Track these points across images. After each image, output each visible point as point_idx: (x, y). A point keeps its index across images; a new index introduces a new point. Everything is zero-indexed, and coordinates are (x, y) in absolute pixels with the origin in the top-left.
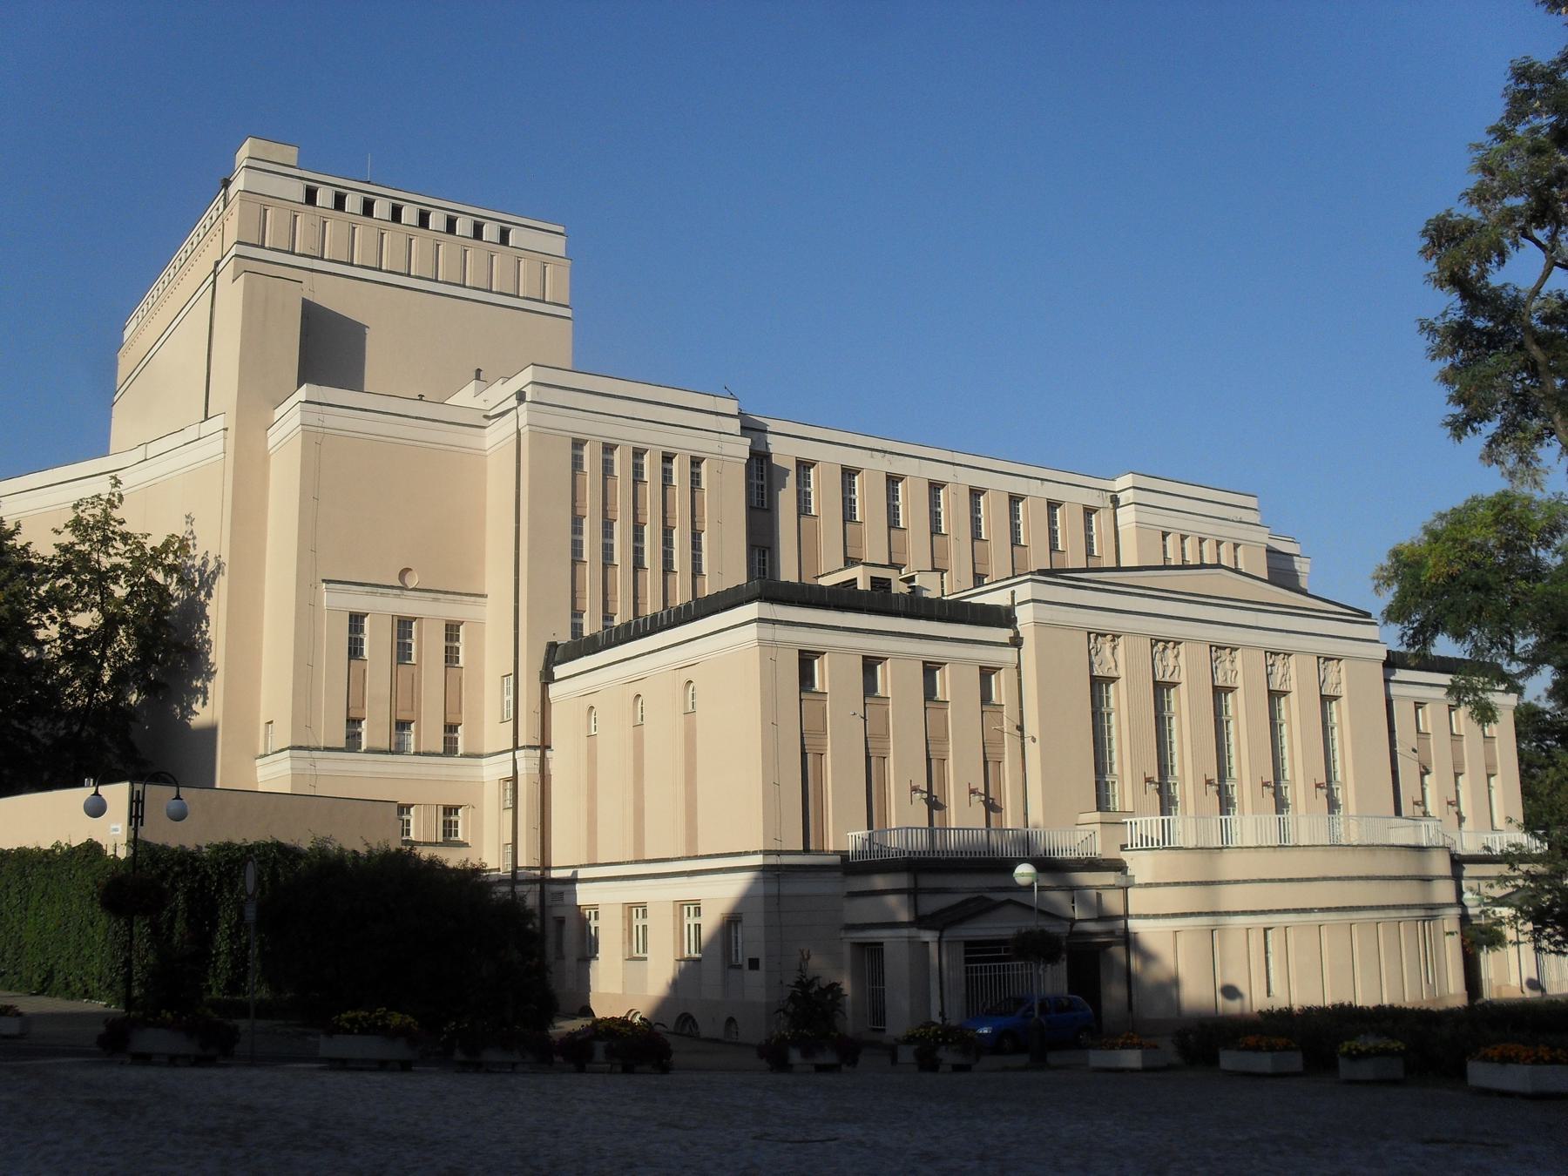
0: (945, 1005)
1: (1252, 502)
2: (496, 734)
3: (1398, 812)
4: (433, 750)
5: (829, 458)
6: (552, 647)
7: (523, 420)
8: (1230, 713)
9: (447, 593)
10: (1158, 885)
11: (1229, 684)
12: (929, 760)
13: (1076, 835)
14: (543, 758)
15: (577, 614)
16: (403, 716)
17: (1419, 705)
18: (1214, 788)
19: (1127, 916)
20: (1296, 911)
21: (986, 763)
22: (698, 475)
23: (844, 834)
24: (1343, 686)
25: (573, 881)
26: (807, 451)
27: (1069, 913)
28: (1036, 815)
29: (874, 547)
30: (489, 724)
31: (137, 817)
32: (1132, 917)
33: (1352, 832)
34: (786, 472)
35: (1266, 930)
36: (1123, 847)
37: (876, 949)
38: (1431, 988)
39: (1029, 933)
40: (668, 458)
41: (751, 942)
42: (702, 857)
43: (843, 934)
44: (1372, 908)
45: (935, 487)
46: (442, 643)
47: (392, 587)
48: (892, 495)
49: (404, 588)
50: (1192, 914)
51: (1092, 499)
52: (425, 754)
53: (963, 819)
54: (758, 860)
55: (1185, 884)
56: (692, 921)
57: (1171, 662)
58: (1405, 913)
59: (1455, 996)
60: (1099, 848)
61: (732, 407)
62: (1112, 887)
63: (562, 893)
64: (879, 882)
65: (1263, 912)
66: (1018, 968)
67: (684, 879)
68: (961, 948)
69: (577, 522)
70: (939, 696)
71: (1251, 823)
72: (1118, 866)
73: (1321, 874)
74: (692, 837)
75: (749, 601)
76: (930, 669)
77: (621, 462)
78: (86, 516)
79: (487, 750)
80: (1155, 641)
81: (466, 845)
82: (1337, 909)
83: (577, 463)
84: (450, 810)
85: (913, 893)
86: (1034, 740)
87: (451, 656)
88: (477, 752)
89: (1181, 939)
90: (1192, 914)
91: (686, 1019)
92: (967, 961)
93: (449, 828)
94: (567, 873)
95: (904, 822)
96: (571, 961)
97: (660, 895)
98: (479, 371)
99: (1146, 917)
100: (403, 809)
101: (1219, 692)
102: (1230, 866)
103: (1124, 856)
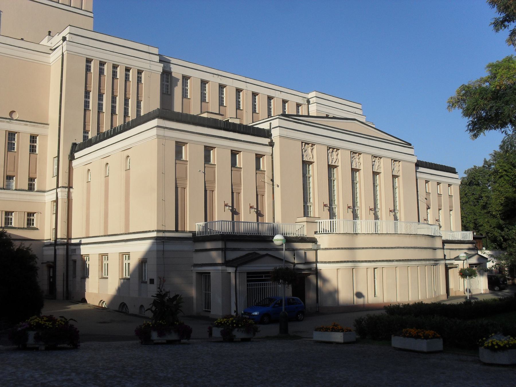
0: (237, 306)
1: (360, 106)
2: (50, 182)
3: (419, 221)
4: (23, 188)
5: (196, 75)
6: (74, 145)
7: (64, 49)
8: (358, 180)
10: (331, 249)
11: (357, 168)
12: (232, 193)
13: (298, 227)
14: (69, 193)
15: (86, 132)
16: (10, 174)
17: (427, 182)
18: (351, 210)
19: (317, 262)
20: (387, 261)
21: (257, 195)
22: (141, 78)
23: (194, 224)
24: (401, 172)
25: (80, 244)
26: (187, 72)
27: (292, 260)
28: (278, 219)
29: (213, 105)
30: (47, 179)
32: (319, 262)
33: (402, 228)
34: (178, 80)
35: (374, 269)
36: (316, 233)
37: (206, 276)
38: (435, 292)
39: (280, 269)
40: (128, 70)
41: (151, 272)
43: (192, 268)
44: (415, 260)
45: (238, 91)
46: (28, 143)
47: (6, 118)
48: (221, 93)
49: (12, 119)
50: (345, 262)
51: (300, 101)
52: (19, 190)
53: (247, 218)
54: (154, 234)
55: (342, 249)
56: (126, 262)
57: (335, 157)
58: (428, 262)
59: (443, 295)
60: (306, 233)
61: (156, 51)
62: (311, 249)
63: (75, 249)
64: (208, 245)
65: (373, 261)
66: (270, 285)
67: (123, 243)
68: (246, 275)
69: (87, 94)
70: (238, 165)
71: (364, 224)
72: (313, 241)
73: (397, 246)
74: (127, 225)
75: (153, 118)
76: (234, 153)
77: (107, 70)
79: (47, 189)
80: (329, 148)
81: (37, 229)
82: (403, 260)
84: (30, 214)
85: (224, 250)
86: (278, 186)
87: (33, 149)
88: (43, 190)
89: (340, 272)
90: (345, 262)
91: (123, 305)
92: (248, 281)
93: (30, 222)
94: (77, 241)
95: (221, 220)
96: (78, 278)
97: (114, 250)
98: (50, 32)
99: (325, 262)
101: (354, 171)
102: (360, 242)
103: (316, 236)
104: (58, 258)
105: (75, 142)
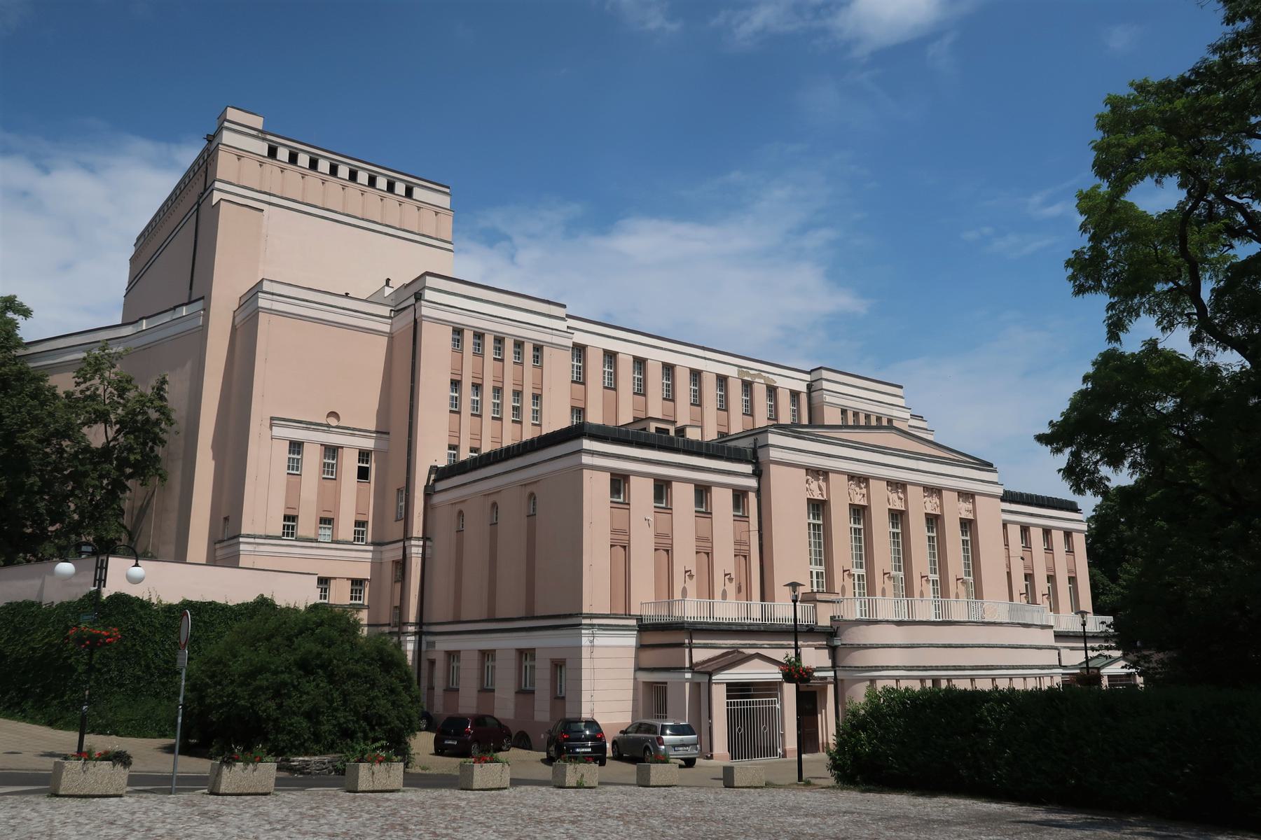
105: (434, 464)
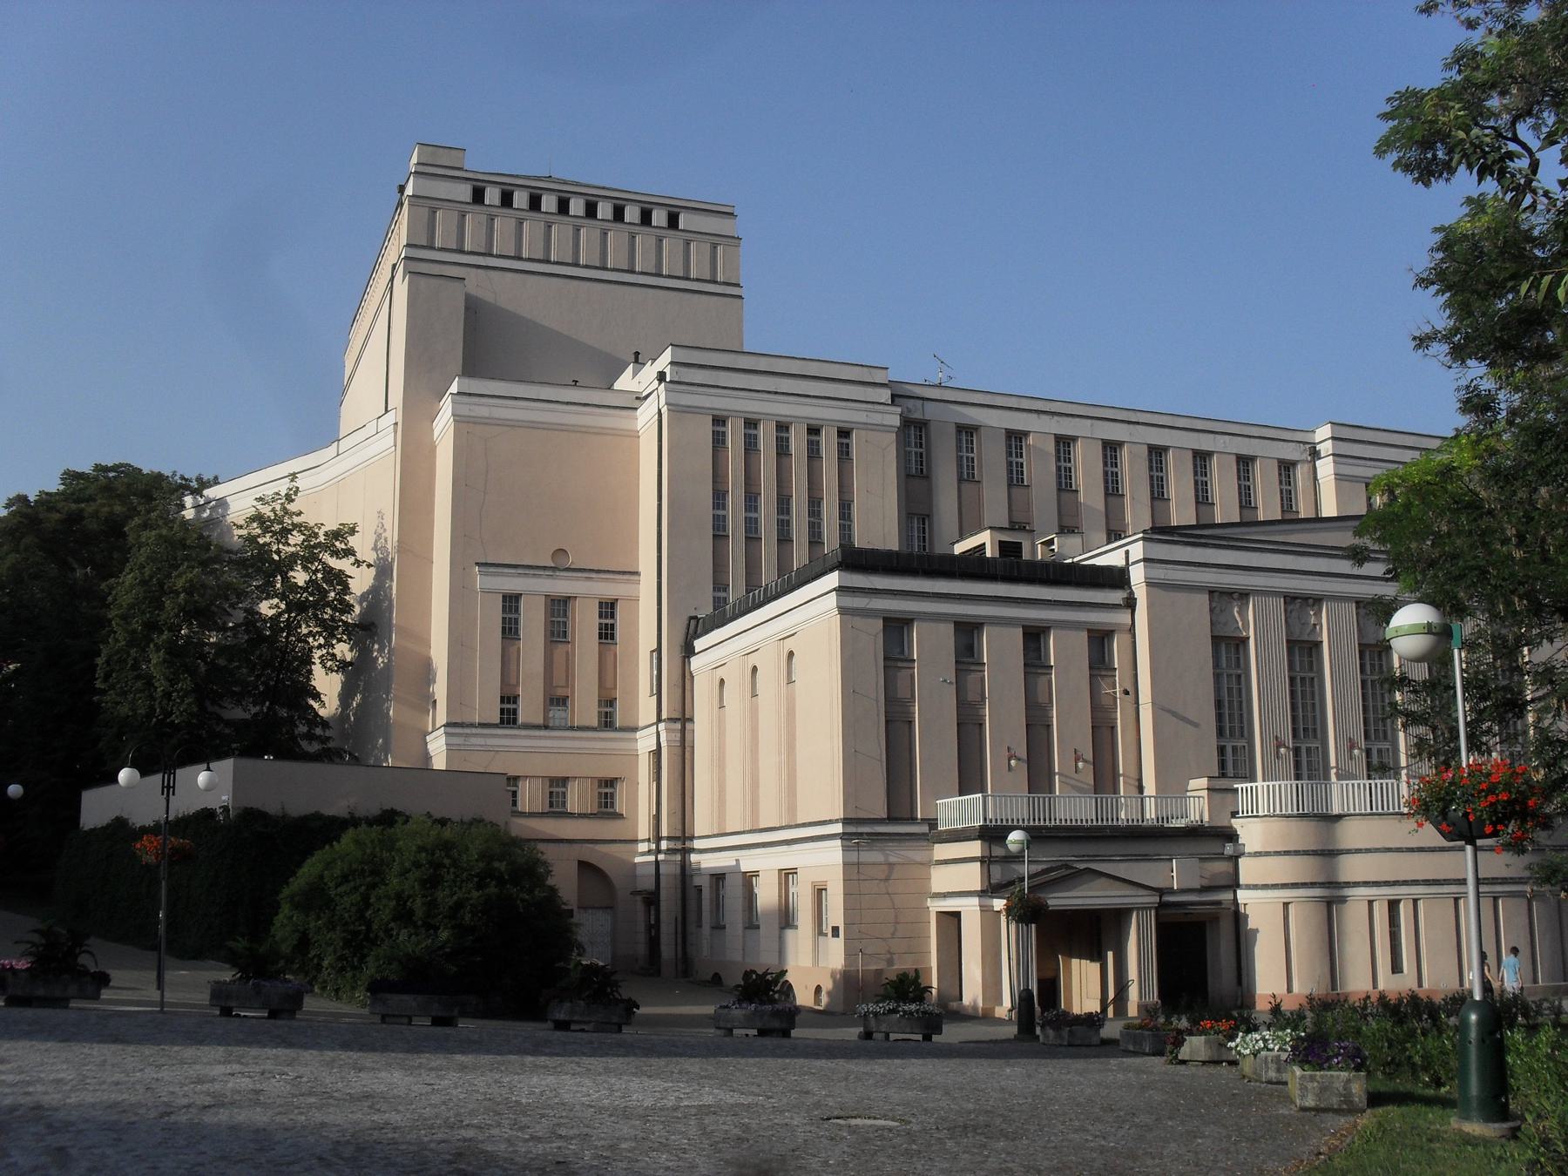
2: (646, 709)
9: (599, 571)
20: (1427, 882)
31: (169, 787)
42: (804, 825)
47: (545, 568)
51: (1289, 452)
69: (719, 497)
75: (832, 570)
77: (797, 442)
78: (266, 511)
79: (641, 724)
80: (1291, 599)
83: (719, 440)
84: (610, 783)
88: (631, 725)
98: (637, 354)
100: (513, 780)
104: (663, 884)
